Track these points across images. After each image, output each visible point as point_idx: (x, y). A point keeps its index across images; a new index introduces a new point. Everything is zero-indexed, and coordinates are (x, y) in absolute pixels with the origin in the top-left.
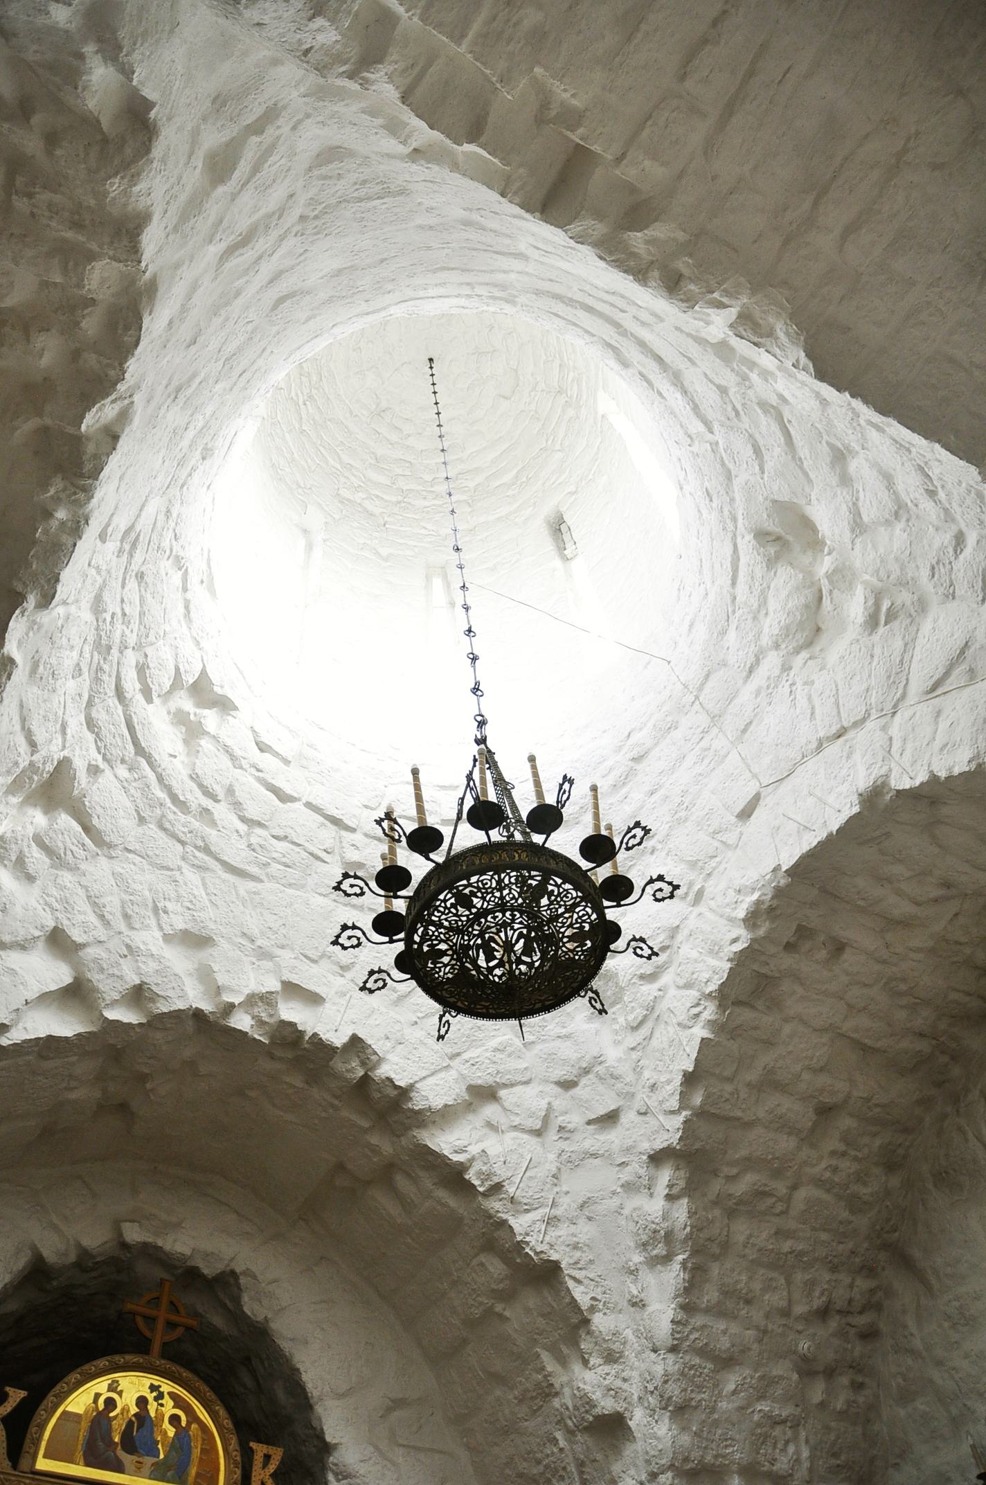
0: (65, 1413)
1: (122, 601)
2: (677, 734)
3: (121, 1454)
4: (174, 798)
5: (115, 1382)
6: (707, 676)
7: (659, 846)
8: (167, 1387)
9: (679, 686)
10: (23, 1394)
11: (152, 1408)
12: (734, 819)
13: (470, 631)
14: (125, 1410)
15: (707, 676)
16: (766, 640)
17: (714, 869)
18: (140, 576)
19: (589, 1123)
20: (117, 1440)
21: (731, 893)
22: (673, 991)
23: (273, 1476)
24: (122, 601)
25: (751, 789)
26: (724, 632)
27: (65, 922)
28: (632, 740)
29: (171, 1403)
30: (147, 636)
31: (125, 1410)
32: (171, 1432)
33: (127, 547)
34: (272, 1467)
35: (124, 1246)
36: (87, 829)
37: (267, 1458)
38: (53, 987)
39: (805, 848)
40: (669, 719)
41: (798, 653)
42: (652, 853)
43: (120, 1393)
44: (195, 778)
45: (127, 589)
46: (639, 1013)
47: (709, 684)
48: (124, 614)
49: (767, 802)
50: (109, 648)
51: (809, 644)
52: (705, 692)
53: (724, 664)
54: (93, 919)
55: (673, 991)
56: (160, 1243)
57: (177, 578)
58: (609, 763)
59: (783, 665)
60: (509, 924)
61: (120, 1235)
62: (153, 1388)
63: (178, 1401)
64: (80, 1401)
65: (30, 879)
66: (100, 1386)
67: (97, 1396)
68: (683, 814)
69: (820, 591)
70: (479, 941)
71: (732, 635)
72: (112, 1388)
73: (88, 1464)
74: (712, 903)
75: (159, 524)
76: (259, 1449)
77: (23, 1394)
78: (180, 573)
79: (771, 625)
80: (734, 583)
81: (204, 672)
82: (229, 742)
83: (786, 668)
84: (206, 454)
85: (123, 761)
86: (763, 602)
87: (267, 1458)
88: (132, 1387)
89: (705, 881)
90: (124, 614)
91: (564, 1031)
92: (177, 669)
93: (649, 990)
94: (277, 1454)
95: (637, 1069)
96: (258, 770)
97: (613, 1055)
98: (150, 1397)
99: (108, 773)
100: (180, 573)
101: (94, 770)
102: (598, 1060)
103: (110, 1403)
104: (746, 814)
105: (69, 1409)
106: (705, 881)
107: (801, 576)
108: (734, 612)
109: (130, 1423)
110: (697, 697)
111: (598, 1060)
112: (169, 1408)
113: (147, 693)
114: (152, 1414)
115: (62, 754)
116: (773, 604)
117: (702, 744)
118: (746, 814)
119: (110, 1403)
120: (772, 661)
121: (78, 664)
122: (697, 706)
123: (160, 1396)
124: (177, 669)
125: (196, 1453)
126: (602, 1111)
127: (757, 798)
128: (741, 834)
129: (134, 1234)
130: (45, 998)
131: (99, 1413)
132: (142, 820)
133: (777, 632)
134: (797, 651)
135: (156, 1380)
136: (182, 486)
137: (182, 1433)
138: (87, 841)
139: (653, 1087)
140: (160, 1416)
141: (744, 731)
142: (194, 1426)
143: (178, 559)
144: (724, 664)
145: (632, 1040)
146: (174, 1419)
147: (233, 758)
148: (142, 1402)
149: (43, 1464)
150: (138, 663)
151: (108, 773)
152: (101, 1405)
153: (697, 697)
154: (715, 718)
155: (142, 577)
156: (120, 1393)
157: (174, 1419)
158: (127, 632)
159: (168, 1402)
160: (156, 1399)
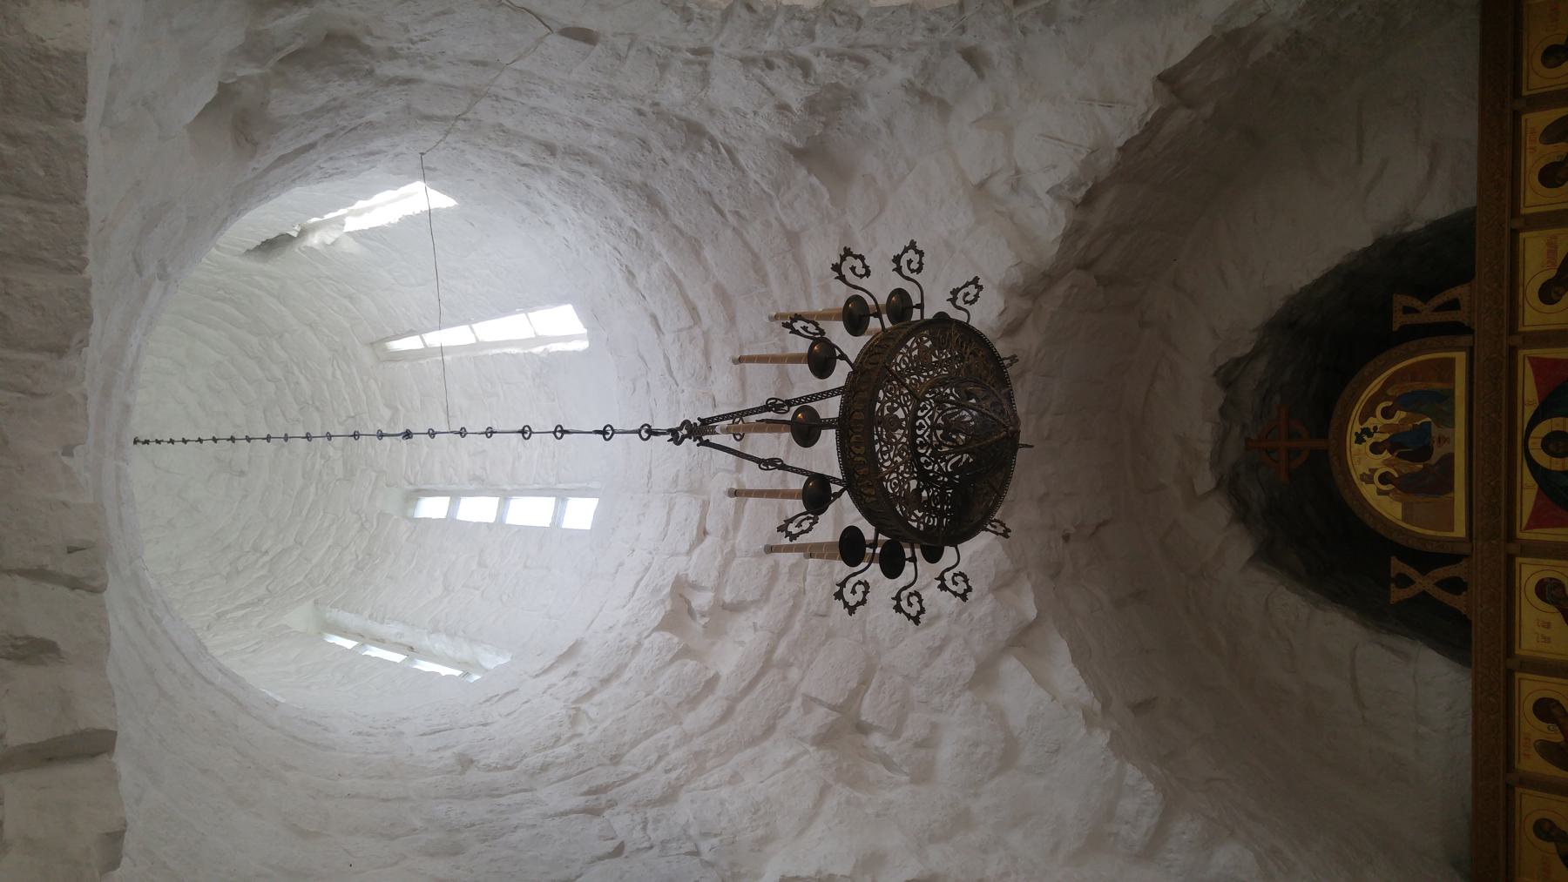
0: (1405, 519)
1: (649, 768)
2: (509, 123)
3: (1434, 459)
4: (795, 607)
5: (1363, 478)
6: (429, 118)
7: (649, 101)
8: (1355, 427)
9: (449, 138)
10: (1394, 561)
11: (1380, 437)
12: (598, 47)
13: (523, 432)
14: (1388, 463)
15: (429, 118)
16: (367, 85)
17: (662, 46)
18: (615, 759)
19: (981, 76)
20: (1420, 466)
21: (691, 27)
22: (818, 43)
23: (1425, 302)
24: (649, 768)
25: (556, 41)
26: (370, 125)
27: (961, 682)
28: (531, 161)
29: (1371, 419)
30: (662, 716)
31: (1388, 463)
32: (1400, 415)
33: (603, 799)
34: (1416, 303)
35: (1218, 486)
36: (864, 682)
37: (1408, 310)
38: (1027, 675)
39: (1068, 656)
40: (492, 135)
41: (369, 47)
42: (657, 104)
43: (1373, 471)
44: (765, 596)
45: (636, 770)
46: (847, 65)
47: (437, 112)
48: (660, 758)
49: (568, 21)
50: (697, 755)
51: (351, 40)
52: (446, 112)
53: (408, 108)
54: (947, 655)
55: (818, 43)
56: (1208, 455)
57: (590, 708)
58: (565, 174)
59: (390, 59)
60: (934, 450)
61: (1209, 493)
62: (1360, 440)
63: (1367, 413)
64: (1390, 508)
65: (934, 727)
66: (1369, 492)
67: (1380, 492)
68: (604, 92)
69: (281, 60)
70: (939, 432)
71: (371, 117)
72: (1368, 479)
73: (1451, 488)
74: (707, 40)
75: (560, 772)
76: (1399, 319)
77: (1394, 561)
78: (584, 706)
79: (340, 89)
80: (312, 146)
81: (658, 628)
82: (714, 574)
83: (393, 55)
84: (466, 762)
85: (785, 678)
86: (324, 110)
87: (1408, 310)
88: (1363, 461)
89: (679, 50)
90: (660, 758)
91: (884, 130)
92: (672, 661)
93: (820, 65)
94: (1400, 300)
95: (913, 47)
96: (727, 530)
97: (898, 73)
98: (1370, 441)
99: (803, 689)
100: (584, 706)
101: (810, 702)
102: (909, 87)
103: (1384, 479)
104: (585, 36)
105: (1399, 516)
106: (679, 50)
107: (274, 91)
108: (343, 128)
109: (1400, 456)
110: (457, 118)
111: (909, 87)
112: (1376, 421)
113: (711, 684)
114: (1387, 436)
115: (811, 749)
116: (322, 99)
117: (511, 95)
118: (585, 36)
119: (1384, 479)
120: (388, 69)
121: (730, 782)
122: (469, 115)
123: (1366, 431)
124: (672, 661)
125: (1418, 386)
126: (966, 69)
127: (568, 32)
128: (615, 35)
129: (1205, 480)
130: (1041, 681)
131: (1398, 486)
132: (830, 635)
133: (354, 83)
134: (366, 50)
135: (1350, 438)
136: (510, 768)
137: (1403, 402)
138: (874, 684)
139: (932, 30)
140: (1387, 428)
141: (484, 64)
142: (1390, 393)
143: (574, 720)
144: (408, 108)
145: (879, 61)
146: (1387, 413)
147: (726, 564)
148: (1376, 449)
149: (1460, 531)
150: (689, 710)
151: (803, 689)
152: (1390, 487)
153: (457, 118)
154: (476, 94)
155: (615, 757)
156: (1373, 471)
157: (1387, 413)
158: (672, 742)
159: (1371, 423)
160: (1370, 435)
